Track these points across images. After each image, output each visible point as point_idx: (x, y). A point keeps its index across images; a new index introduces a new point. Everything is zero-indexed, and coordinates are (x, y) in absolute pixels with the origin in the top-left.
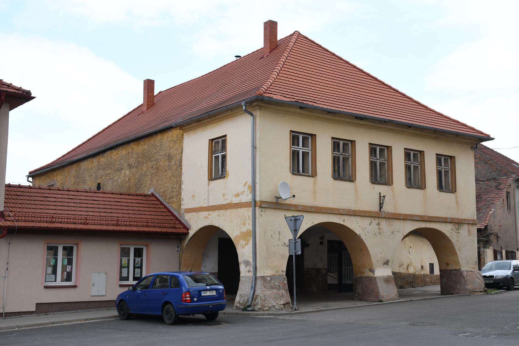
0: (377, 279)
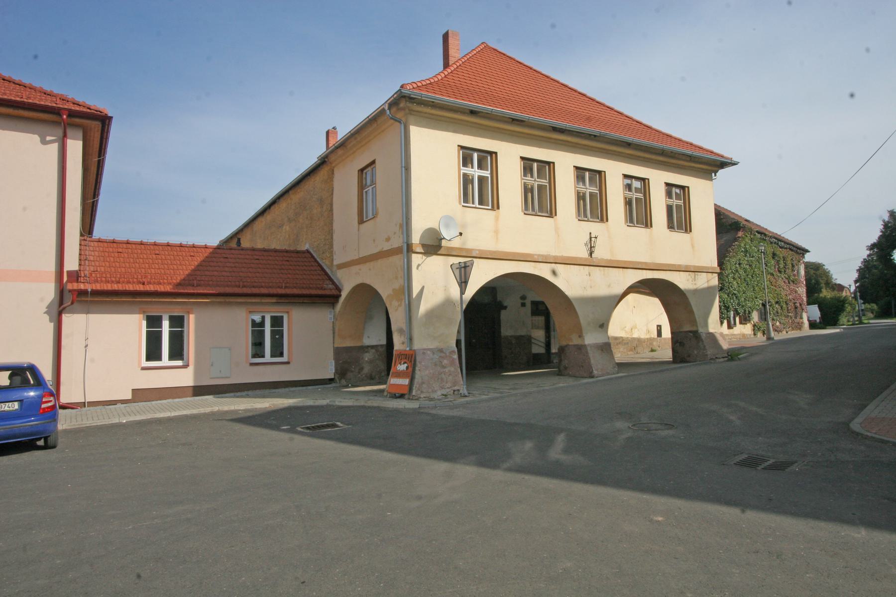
0: (589, 348)
